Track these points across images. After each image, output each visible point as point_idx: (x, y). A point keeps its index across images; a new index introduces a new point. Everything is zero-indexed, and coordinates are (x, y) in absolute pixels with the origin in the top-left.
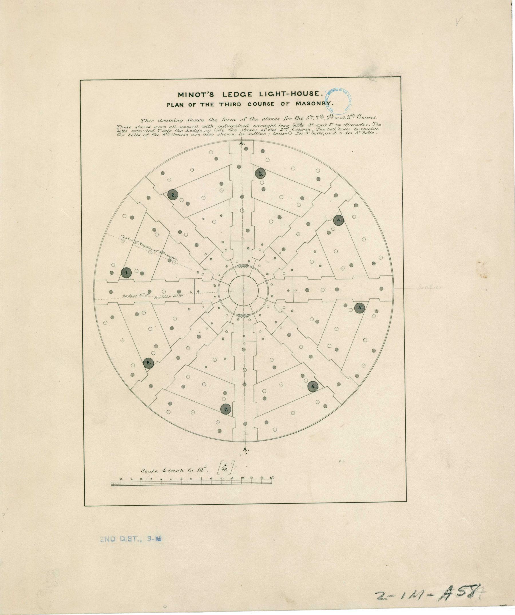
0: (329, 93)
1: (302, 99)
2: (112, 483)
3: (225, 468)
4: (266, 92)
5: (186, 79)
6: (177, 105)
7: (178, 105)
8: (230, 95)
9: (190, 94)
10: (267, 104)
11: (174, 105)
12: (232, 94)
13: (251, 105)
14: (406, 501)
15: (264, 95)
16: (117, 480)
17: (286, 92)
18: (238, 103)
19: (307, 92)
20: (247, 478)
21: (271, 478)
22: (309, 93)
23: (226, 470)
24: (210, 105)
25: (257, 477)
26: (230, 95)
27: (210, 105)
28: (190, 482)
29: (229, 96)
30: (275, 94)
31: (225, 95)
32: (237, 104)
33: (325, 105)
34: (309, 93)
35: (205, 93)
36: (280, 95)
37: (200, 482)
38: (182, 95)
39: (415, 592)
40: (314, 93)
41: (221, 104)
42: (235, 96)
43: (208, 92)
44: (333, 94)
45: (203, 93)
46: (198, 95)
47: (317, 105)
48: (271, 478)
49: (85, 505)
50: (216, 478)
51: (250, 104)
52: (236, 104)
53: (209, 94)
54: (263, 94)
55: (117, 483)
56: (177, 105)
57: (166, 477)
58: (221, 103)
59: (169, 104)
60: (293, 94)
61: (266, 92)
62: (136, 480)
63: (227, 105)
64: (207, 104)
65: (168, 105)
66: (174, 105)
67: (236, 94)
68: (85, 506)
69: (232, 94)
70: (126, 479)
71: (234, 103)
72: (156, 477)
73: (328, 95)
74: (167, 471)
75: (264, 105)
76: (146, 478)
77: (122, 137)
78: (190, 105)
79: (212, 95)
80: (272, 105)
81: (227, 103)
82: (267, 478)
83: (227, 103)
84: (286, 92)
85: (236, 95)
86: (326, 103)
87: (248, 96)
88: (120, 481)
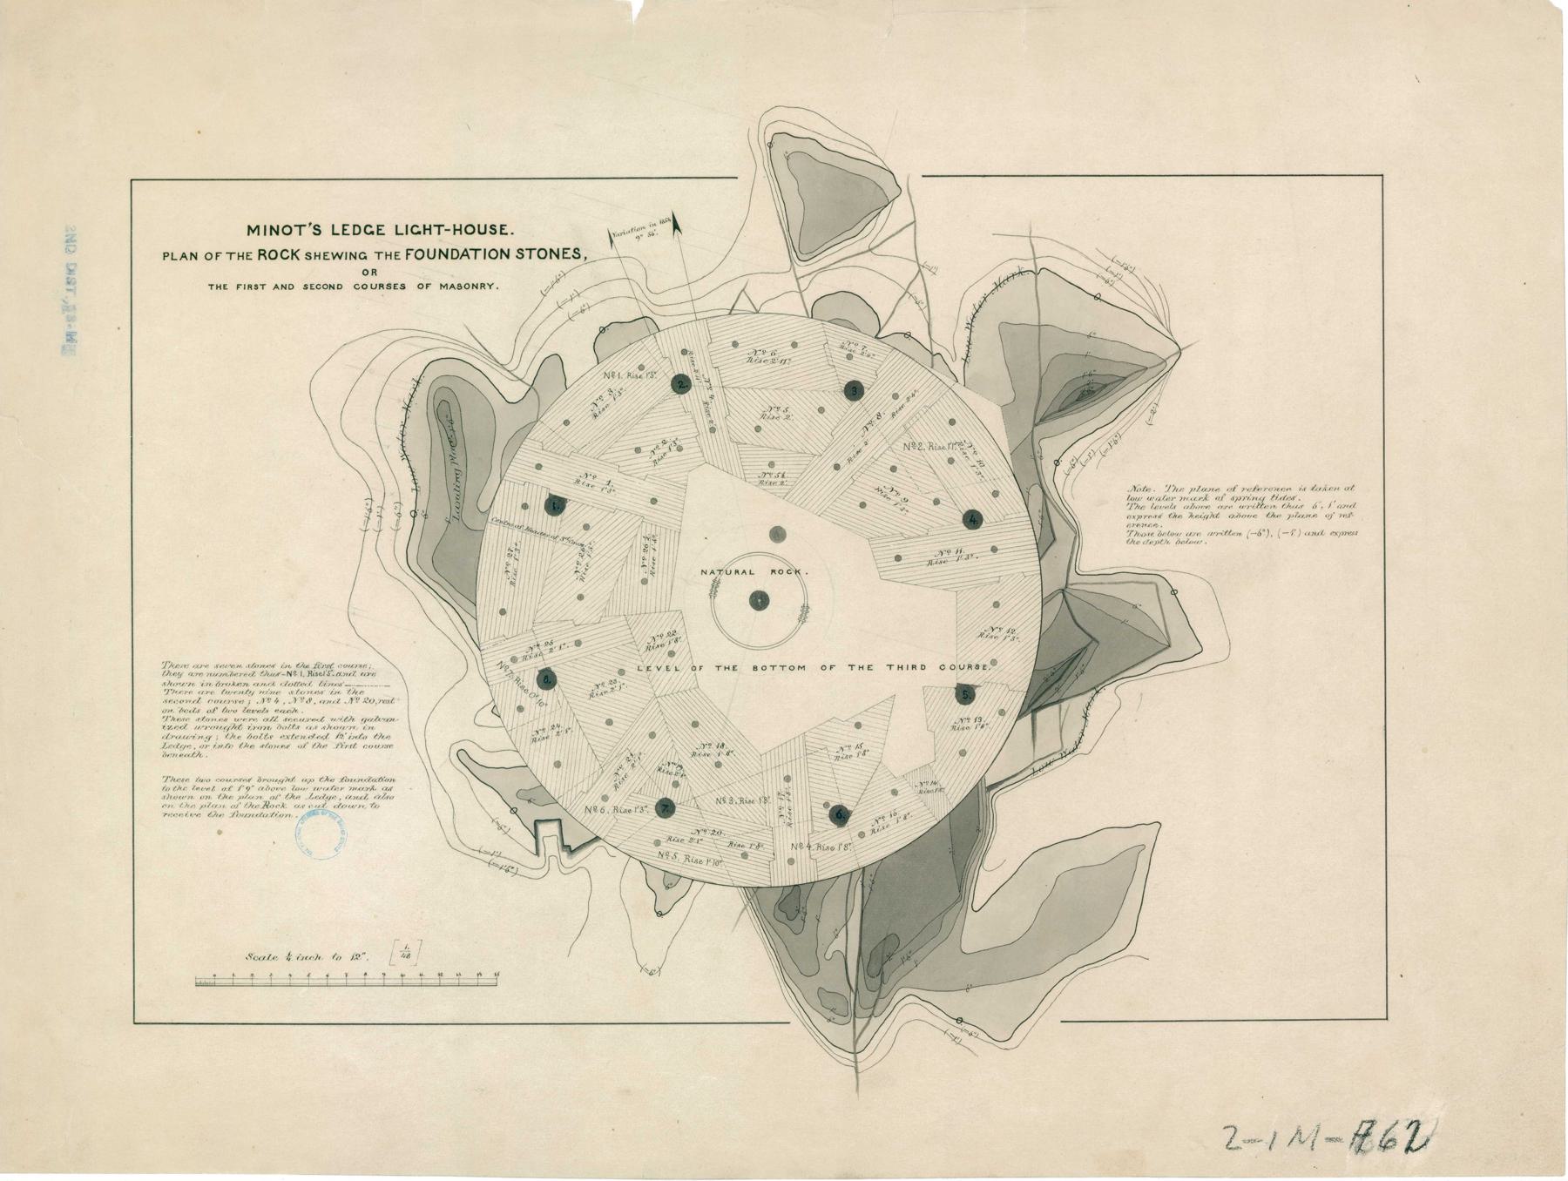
1: (489, 242)
2: (198, 981)
3: (406, 954)
4: (407, 226)
6: (184, 256)
7: (185, 257)
10: (385, 286)
11: (177, 255)
12: (349, 230)
15: (404, 232)
16: (207, 976)
17: (443, 226)
18: (452, 250)
19: (485, 226)
20: (449, 975)
22: (488, 229)
23: (408, 956)
24: (393, 255)
25: (449, 975)
26: (380, 232)
27: (393, 255)
29: (343, 234)
30: (421, 229)
31: (399, 232)
32: (267, 255)
34: (488, 229)
35: (304, 226)
36: (430, 233)
38: (256, 232)
40: (498, 229)
41: (298, 228)
42: (354, 234)
45: (300, 226)
46: (287, 230)
48: (497, 975)
50: (393, 975)
54: (402, 229)
56: (184, 256)
57: (299, 970)
58: (379, 253)
59: (165, 255)
61: (407, 226)
63: (389, 257)
64: (241, 254)
66: (177, 255)
67: (357, 230)
69: (349, 230)
71: (262, 252)
72: (280, 970)
74: (293, 958)
75: (262, 257)
77: (1177, 519)
78: (291, 287)
79: (317, 230)
80: (501, 233)
81: (388, 253)
82: (488, 976)
83: (388, 253)
84: (443, 226)
86: (487, 287)
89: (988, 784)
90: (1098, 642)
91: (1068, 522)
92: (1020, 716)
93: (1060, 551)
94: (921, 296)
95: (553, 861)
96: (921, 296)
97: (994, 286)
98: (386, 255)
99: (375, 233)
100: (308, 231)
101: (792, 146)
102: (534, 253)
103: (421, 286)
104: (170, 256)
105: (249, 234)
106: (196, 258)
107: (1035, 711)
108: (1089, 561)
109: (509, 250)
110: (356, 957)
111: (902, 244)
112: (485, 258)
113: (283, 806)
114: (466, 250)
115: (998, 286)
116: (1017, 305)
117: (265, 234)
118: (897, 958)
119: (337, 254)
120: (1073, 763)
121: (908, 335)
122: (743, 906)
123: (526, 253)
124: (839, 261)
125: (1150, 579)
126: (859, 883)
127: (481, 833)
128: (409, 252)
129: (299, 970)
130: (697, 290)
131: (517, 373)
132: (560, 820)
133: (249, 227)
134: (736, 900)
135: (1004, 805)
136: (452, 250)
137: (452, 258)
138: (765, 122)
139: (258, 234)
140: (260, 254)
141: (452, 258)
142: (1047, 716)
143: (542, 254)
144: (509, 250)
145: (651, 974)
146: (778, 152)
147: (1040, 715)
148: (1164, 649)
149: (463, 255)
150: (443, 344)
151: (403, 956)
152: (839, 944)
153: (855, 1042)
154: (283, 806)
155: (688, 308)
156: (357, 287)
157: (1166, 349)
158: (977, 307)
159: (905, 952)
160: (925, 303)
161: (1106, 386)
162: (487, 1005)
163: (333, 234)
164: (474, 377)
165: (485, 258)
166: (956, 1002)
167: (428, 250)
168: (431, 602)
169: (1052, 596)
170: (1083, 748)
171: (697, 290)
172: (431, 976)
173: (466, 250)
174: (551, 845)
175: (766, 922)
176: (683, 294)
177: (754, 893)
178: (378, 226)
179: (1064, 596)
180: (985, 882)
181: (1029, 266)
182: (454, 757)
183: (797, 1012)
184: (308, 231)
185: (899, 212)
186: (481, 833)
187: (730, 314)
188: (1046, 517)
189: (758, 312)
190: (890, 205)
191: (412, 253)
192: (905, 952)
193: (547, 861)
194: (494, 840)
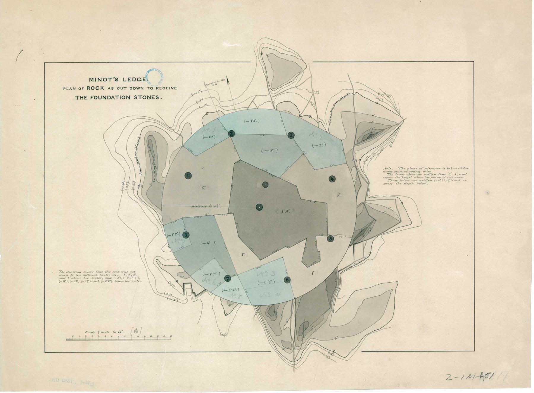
0: (148, 72)
3: (136, 331)
5: (474, 97)
6: (71, 89)
8: (129, 80)
9: (98, 79)
11: (69, 89)
12: (131, 79)
13: (99, 89)
14: (44, 63)
18: (108, 96)
21: (171, 336)
24: (159, 88)
25: (154, 337)
27: (159, 88)
28: (118, 339)
29: (128, 81)
32: (90, 88)
33: (103, 89)
35: (112, 78)
37: (124, 339)
38: (92, 80)
39: (357, 197)
41: (77, 97)
42: (133, 81)
43: (114, 77)
44: (151, 72)
45: (110, 78)
46: (105, 80)
47: (101, 78)
48: (171, 336)
49: (46, 352)
51: (118, 88)
52: (90, 88)
53: (115, 79)
55: (70, 339)
59: (64, 88)
60: (294, 363)
62: (82, 336)
65: (64, 89)
66: (69, 89)
68: (45, 352)
69: (131, 79)
70: (76, 337)
71: (88, 87)
73: (147, 73)
75: (157, 89)
76: (89, 336)
79: (117, 80)
84: (119, 96)
85: (134, 80)
87: (143, 81)
88: (72, 337)
89: (339, 270)
90: (376, 221)
91: (365, 180)
92: (350, 246)
93: (362, 191)
94: (313, 102)
95: (189, 297)
96: (313, 102)
97: (339, 99)
98: (81, 98)
99: (142, 80)
100: (113, 80)
101: (270, 51)
102: (141, 97)
103: (131, 88)
104: (66, 88)
105: (90, 81)
106: (143, 89)
107: (354, 244)
108: (373, 192)
109: (129, 96)
110: (120, 332)
111: (307, 85)
112: (120, 99)
113: (402, 172)
114: (113, 96)
115: (341, 99)
116: (346, 106)
117: (96, 81)
118: (309, 329)
119: (138, 88)
120: (368, 263)
121: (310, 116)
122: (255, 313)
123: (138, 97)
124: (284, 91)
125: (394, 198)
126: (294, 304)
127: (165, 288)
128: (92, 97)
129: (102, 336)
130: (236, 102)
131: (175, 130)
132: (191, 283)
133: (90, 79)
134: (252, 310)
135: (346, 278)
136: (108, 96)
137: (108, 99)
138: (259, 46)
139: (93, 81)
140: (88, 88)
141: (108, 99)
142: (358, 247)
143: (144, 97)
144: (129, 96)
145: (224, 336)
146: (264, 55)
147: (356, 246)
148: (399, 223)
149: (112, 98)
150: (148, 120)
151: (135, 332)
152: (288, 325)
153: (294, 359)
154: (402, 172)
155: (232, 108)
156: (118, 88)
157: (398, 120)
158: (334, 105)
159: (311, 326)
160: (315, 104)
161: (377, 133)
162: (165, 346)
163: (124, 81)
164: (162, 132)
165: (120, 99)
166: (331, 345)
167: (99, 96)
168: (145, 208)
169: (360, 204)
170: (371, 257)
171: (236, 102)
172: (148, 337)
173: (113, 96)
174: (189, 292)
175: (263, 316)
176: (231, 103)
177: (258, 308)
178: (143, 78)
179: (364, 205)
180: (338, 303)
181: (352, 91)
182: (155, 262)
183: (275, 349)
184: (113, 80)
185: (306, 74)
186: (165, 288)
187: (248, 109)
188: (358, 178)
189: (258, 109)
190: (303, 72)
191: (93, 97)
192: (311, 326)
193: (187, 298)
194: (169, 289)
